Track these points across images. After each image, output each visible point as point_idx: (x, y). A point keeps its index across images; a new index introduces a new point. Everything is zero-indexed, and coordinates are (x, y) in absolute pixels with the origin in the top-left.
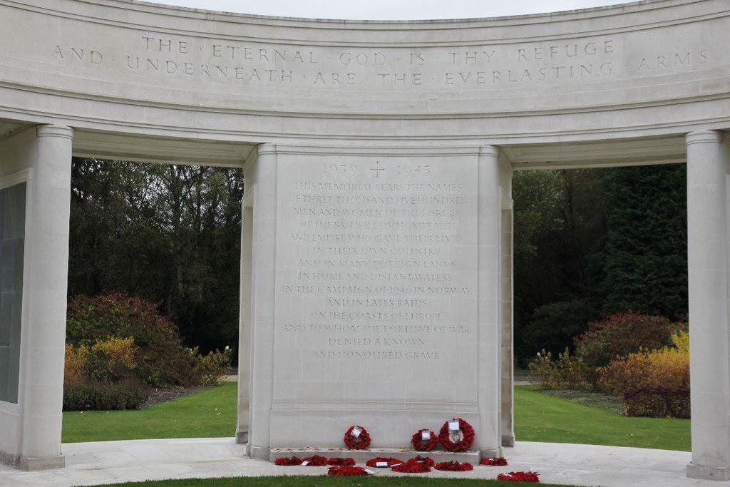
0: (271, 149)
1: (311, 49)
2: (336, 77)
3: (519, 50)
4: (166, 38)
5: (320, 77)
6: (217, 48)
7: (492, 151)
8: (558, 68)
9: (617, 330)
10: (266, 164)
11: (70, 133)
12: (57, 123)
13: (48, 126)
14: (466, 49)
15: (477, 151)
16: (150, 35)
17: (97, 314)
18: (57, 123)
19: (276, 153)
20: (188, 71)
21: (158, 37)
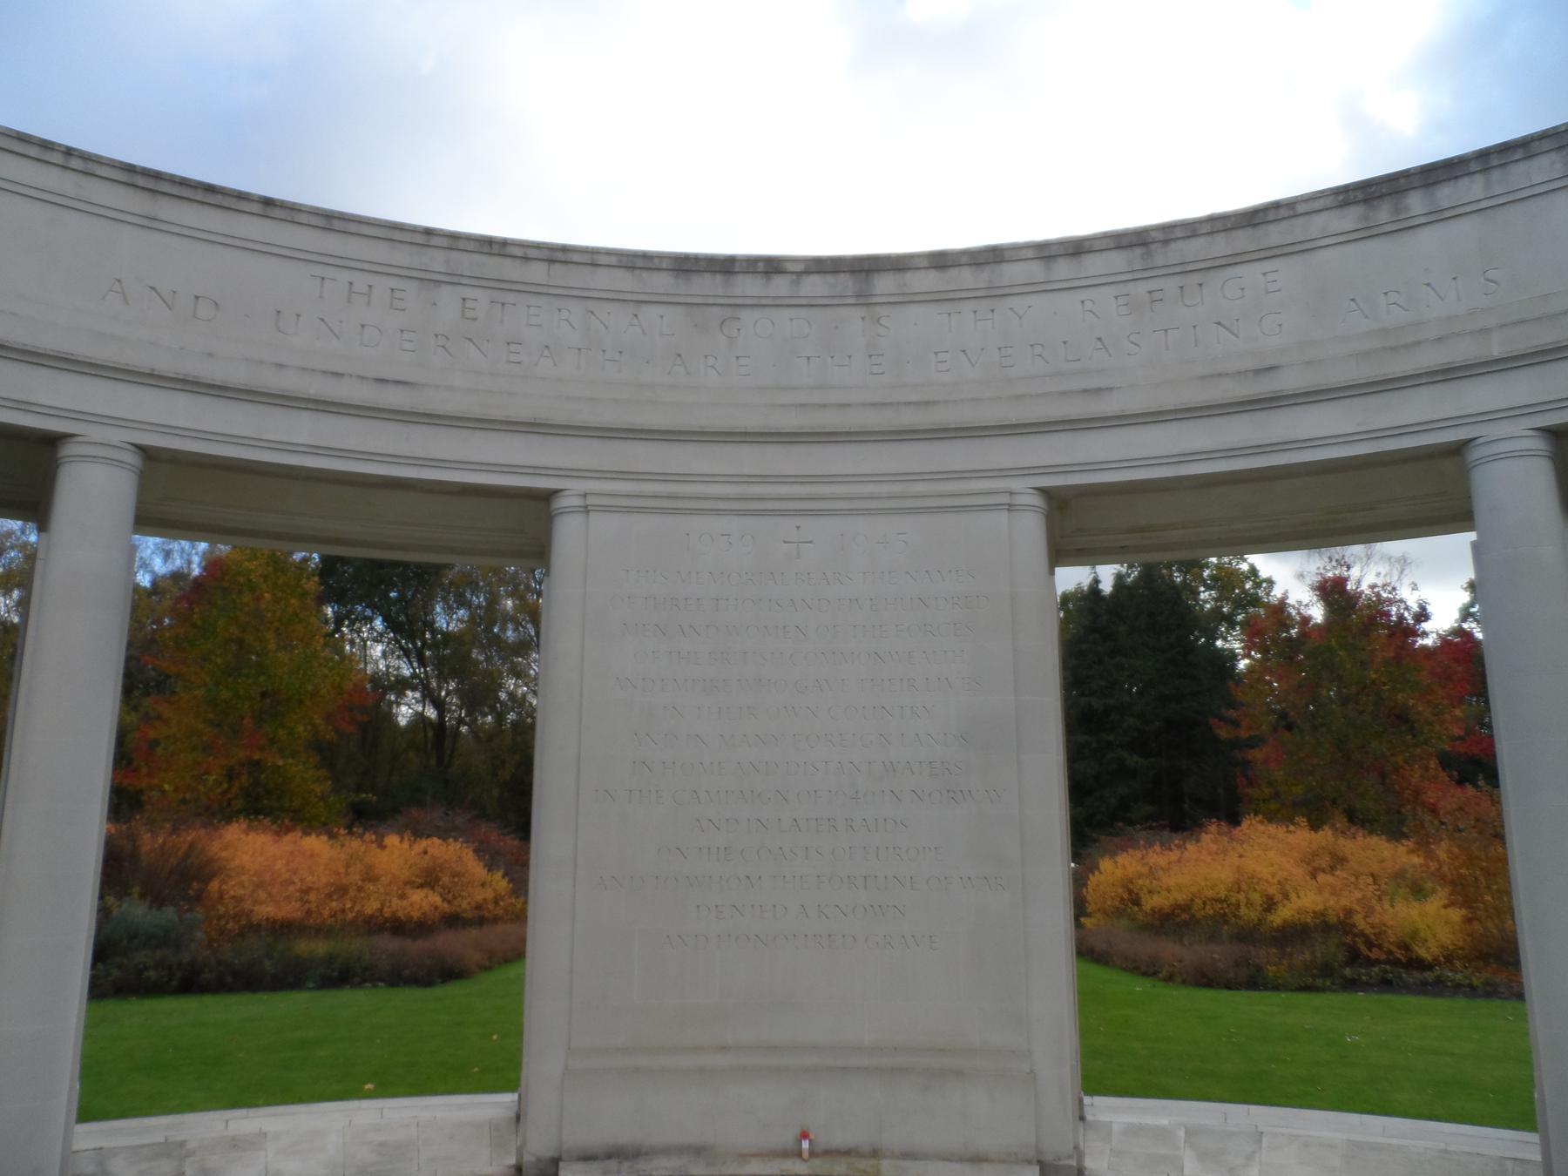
0: (577, 502)
1: (659, 309)
2: (711, 361)
3: (1083, 302)
4: (361, 281)
5: (635, 321)
6: (469, 304)
7: (1037, 501)
8: (1166, 331)
9: (422, 600)
10: (569, 536)
11: (132, 459)
12: (96, 433)
13: (80, 439)
14: (971, 305)
15: (1005, 499)
16: (330, 272)
17: (1306, 881)
18: (96, 433)
19: (586, 510)
20: (407, 346)
21: (345, 276)
